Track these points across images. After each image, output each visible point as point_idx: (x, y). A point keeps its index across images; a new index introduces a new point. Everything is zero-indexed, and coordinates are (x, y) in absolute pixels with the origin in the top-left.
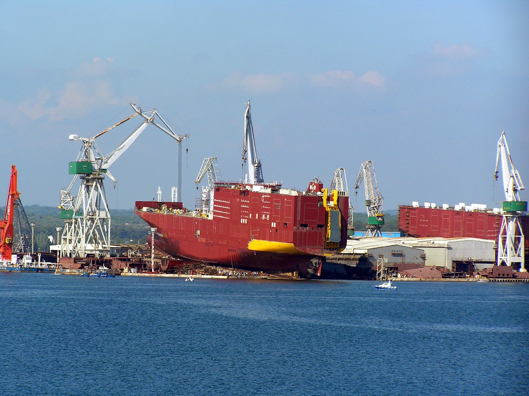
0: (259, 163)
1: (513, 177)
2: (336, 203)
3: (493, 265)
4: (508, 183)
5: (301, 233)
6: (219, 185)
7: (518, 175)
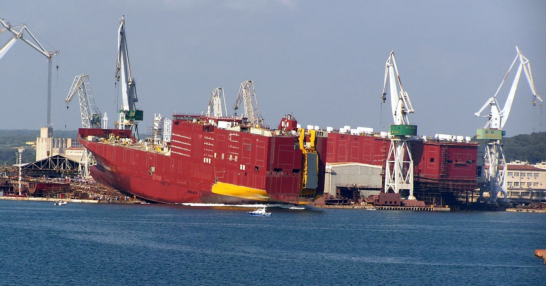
0: (133, 82)
1: (402, 99)
2: (313, 145)
3: (380, 192)
4: (396, 105)
5: (274, 178)
6: (178, 118)
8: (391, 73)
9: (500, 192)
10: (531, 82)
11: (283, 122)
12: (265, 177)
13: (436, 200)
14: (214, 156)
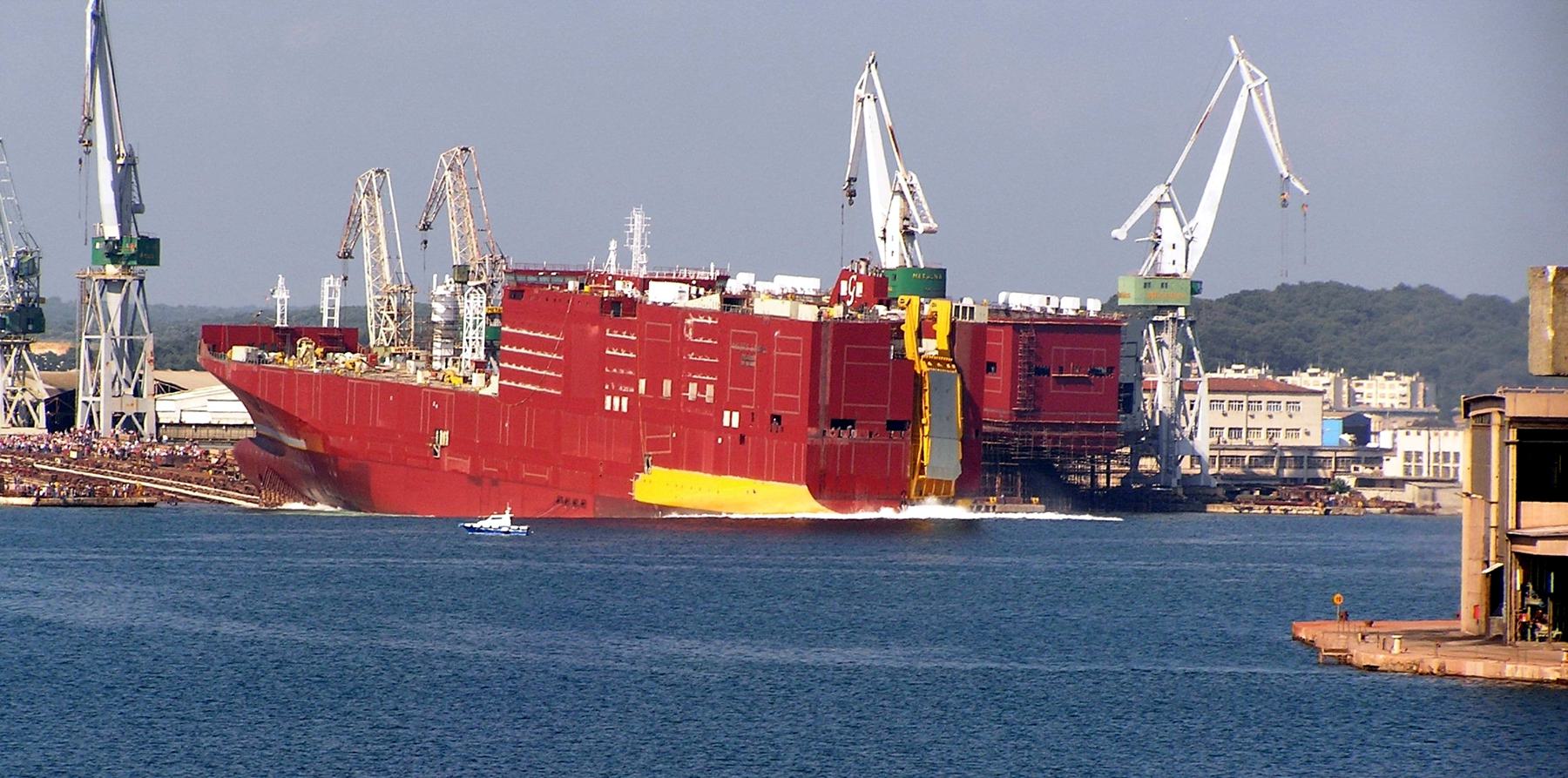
1: (902, 193)
2: (945, 347)
4: (884, 210)
5: (832, 448)
6: (521, 279)
8: (870, 119)
9: (1187, 459)
10: (1273, 139)
11: (844, 284)
12: (804, 447)
13: (1005, 482)
14: (637, 389)
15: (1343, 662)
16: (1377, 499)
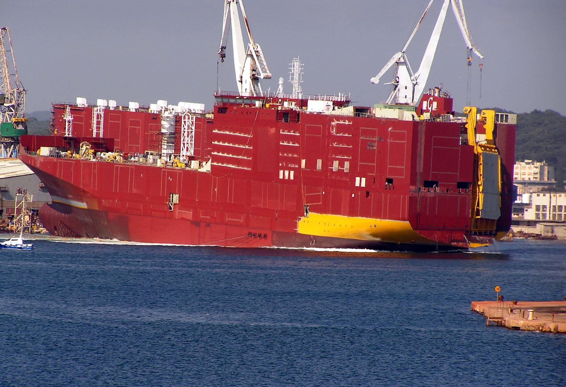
1: (252, 56)
2: (491, 137)
4: (242, 66)
5: (424, 199)
6: (225, 100)
7: (261, 52)
11: (425, 103)
12: (407, 198)
14: (300, 165)
15: (500, 325)
16: (521, 232)
